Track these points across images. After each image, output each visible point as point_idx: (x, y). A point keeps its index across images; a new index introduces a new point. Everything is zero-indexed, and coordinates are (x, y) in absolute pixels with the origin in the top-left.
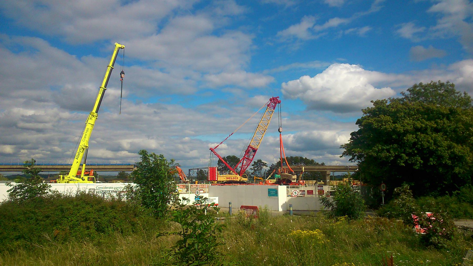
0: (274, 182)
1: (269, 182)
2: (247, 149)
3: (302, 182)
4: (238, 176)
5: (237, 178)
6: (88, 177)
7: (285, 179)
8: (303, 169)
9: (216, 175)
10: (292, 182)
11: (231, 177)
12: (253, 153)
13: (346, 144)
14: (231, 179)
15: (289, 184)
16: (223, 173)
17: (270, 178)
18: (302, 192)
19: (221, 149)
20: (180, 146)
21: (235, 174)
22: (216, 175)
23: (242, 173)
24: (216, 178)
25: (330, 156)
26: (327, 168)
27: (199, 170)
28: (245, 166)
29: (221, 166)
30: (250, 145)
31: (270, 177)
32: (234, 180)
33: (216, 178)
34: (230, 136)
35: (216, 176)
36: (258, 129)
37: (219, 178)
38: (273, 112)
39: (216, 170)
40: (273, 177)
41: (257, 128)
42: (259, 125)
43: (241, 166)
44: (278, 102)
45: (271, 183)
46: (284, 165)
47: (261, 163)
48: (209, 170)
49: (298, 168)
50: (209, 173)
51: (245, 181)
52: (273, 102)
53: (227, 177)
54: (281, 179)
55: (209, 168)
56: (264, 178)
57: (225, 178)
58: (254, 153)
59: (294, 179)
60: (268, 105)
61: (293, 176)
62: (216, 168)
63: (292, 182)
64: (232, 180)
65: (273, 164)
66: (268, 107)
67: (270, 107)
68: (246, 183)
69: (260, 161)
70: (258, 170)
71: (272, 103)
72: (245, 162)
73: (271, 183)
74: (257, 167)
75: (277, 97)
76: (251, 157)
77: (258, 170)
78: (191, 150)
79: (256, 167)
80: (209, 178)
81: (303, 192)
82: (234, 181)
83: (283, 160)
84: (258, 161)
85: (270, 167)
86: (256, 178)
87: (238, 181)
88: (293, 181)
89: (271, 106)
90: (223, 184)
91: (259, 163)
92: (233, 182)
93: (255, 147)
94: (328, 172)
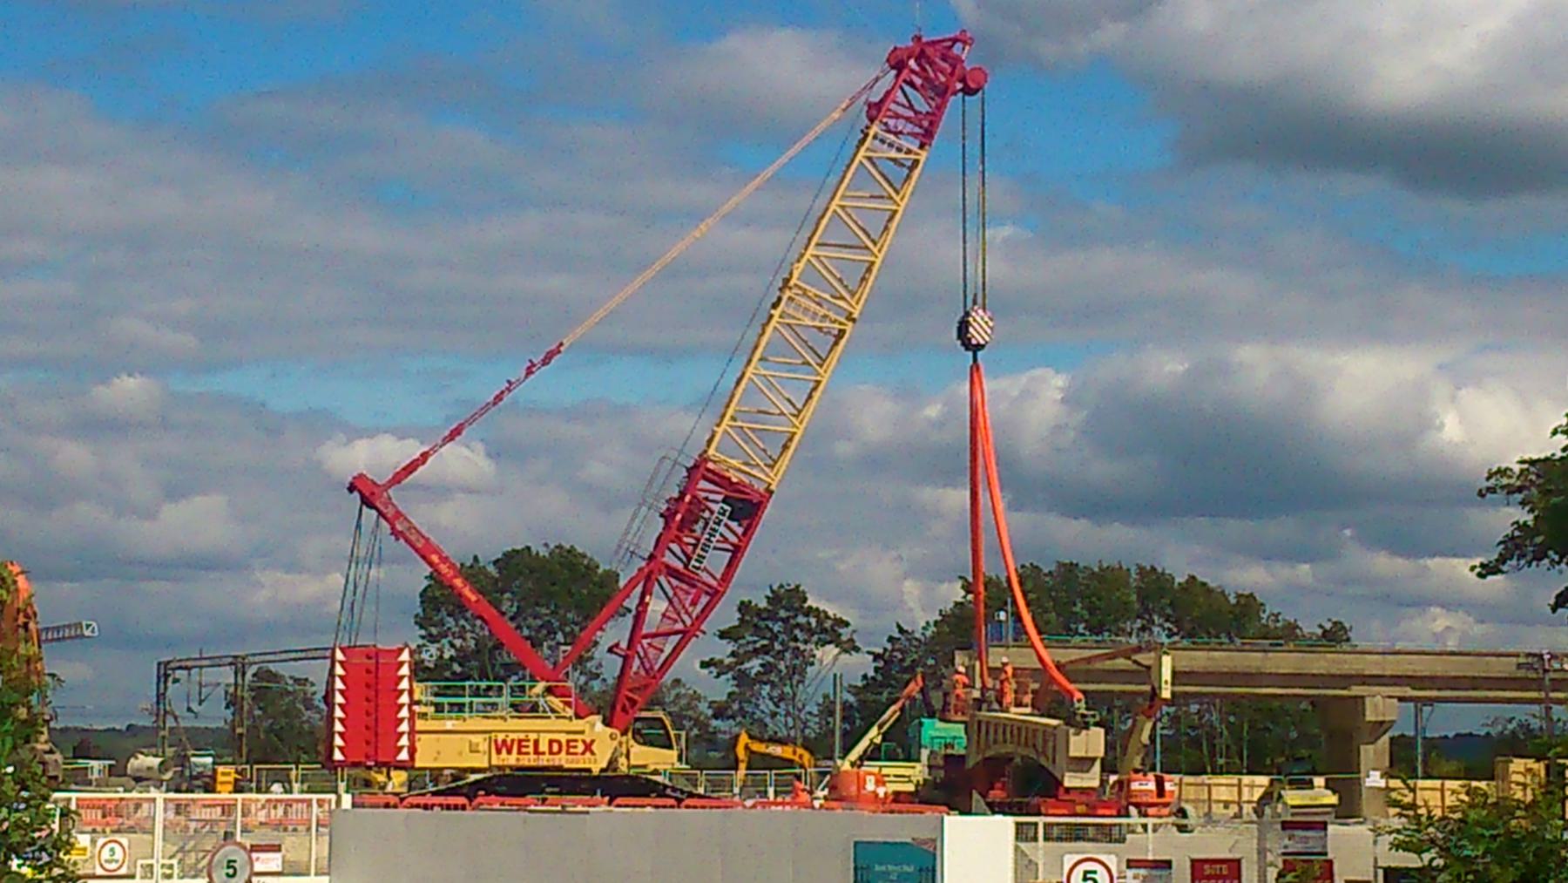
0: (911, 788)
1: (861, 784)
2: (682, 494)
3: (1152, 786)
4: (599, 726)
5: (588, 747)
6: (1018, 824)
7: (1009, 759)
8: (1167, 674)
9: (404, 713)
10: (1060, 783)
11: (533, 736)
12: (734, 525)
13: (1532, 462)
14: (536, 752)
15: (1036, 800)
16: (467, 700)
17: (873, 754)
18: (1143, 872)
19: (441, 491)
20: (75, 456)
21: (570, 712)
22: (404, 713)
23: (633, 702)
24: (404, 741)
25: (1384, 564)
26: (1370, 666)
27: (249, 676)
28: (657, 642)
29: (444, 641)
30: (703, 458)
31: (878, 740)
32: (563, 760)
33: (404, 741)
34: (529, 372)
35: (404, 727)
36: (776, 313)
37: (423, 742)
38: (917, 172)
39: (405, 670)
40: (900, 745)
41: (775, 306)
42: (787, 281)
43: (624, 645)
44: (959, 86)
45: (881, 791)
46: (998, 639)
47: (801, 619)
48: (339, 670)
49: (1121, 663)
50: (339, 699)
51: (656, 772)
52: (918, 81)
53: (501, 737)
54: (970, 763)
55: (339, 656)
56: (820, 747)
57: (484, 747)
58: (740, 531)
59: (1083, 763)
60: (870, 106)
61: (1073, 739)
62: (405, 656)
63: (1067, 783)
64: (545, 761)
65: (901, 630)
66: (872, 120)
67: (891, 122)
68: (658, 790)
69: (788, 600)
70: (773, 677)
71: (907, 88)
72: (657, 606)
73: (881, 791)
74: (765, 650)
75: (955, 41)
76: (716, 561)
77: (773, 677)
78: (175, 493)
79: (756, 652)
80: (338, 741)
81: (1154, 872)
82: (560, 768)
83: (998, 596)
84: (775, 599)
85: (877, 657)
86: (757, 747)
87: (596, 771)
88: (1070, 781)
89: (897, 116)
90: (461, 800)
91: (783, 614)
92: (552, 782)
93: (746, 480)
94: (1379, 705)
